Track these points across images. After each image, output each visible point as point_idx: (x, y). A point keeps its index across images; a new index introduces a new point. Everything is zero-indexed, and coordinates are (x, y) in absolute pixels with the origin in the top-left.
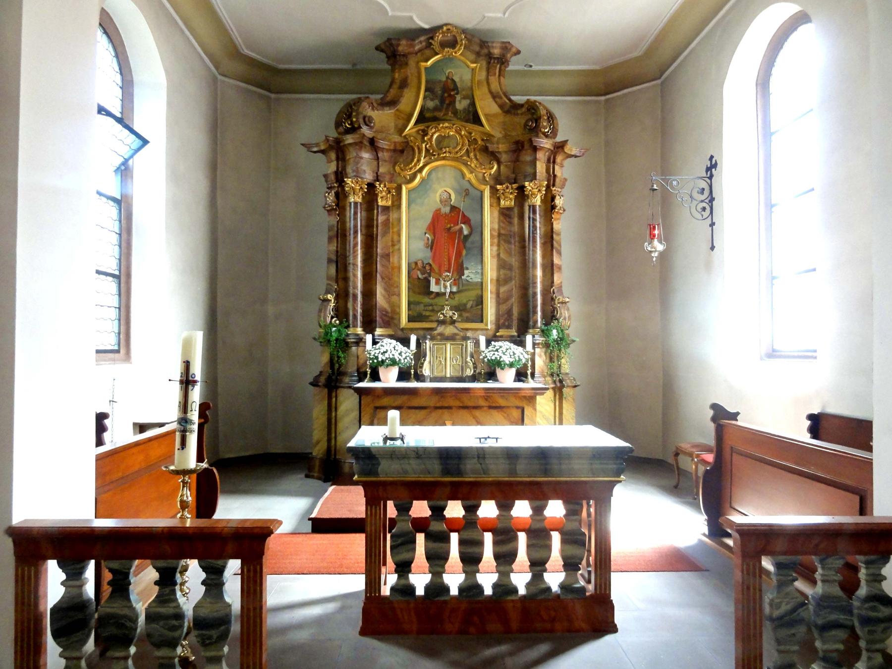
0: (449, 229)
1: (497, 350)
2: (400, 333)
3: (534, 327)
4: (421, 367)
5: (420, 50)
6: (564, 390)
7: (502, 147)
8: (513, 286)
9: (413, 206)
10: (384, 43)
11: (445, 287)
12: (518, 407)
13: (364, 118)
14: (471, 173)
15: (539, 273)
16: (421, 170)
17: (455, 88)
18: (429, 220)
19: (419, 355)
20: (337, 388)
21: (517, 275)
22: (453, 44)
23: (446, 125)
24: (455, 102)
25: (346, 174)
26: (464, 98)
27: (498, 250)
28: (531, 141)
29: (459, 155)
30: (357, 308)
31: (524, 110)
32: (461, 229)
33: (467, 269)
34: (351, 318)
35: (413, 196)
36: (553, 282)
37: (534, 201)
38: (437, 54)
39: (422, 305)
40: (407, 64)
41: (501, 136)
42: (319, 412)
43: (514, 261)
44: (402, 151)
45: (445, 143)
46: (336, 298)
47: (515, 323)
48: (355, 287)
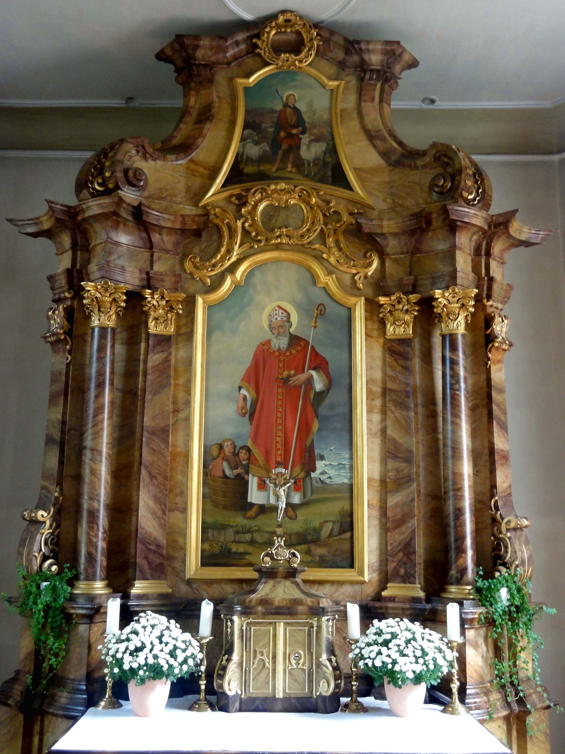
0: (286, 380)
2: (184, 589)
3: (459, 581)
4: (222, 677)
5: (236, 58)
6: (530, 720)
7: (389, 226)
8: (415, 493)
9: (217, 335)
10: (171, 45)
11: (278, 497)
14: (330, 273)
15: (466, 468)
16: (232, 269)
17: (300, 122)
19: (219, 648)
21: (422, 472)
22: (296, 47)
23: (282, 185)
24: (298, 147)
25: (88, 274)
26: (318, 139)
27: (383, 420)
28: (445, 211)
29: (305, 241)
30: (95, 538)
31: (427, 159)
32: (309, 382)
33: (322, 458)
34: (83, 559)
35: (218, 315)
36: (493, 486)
37: (453, 325)
38: (267, 64)
39: (230, 532)
40: (211, 81)
43: (416, 444)
44: (197, 234)
45: (280, 221)
46: (57, 518)
47: (419, 570)
48: (94, 497)
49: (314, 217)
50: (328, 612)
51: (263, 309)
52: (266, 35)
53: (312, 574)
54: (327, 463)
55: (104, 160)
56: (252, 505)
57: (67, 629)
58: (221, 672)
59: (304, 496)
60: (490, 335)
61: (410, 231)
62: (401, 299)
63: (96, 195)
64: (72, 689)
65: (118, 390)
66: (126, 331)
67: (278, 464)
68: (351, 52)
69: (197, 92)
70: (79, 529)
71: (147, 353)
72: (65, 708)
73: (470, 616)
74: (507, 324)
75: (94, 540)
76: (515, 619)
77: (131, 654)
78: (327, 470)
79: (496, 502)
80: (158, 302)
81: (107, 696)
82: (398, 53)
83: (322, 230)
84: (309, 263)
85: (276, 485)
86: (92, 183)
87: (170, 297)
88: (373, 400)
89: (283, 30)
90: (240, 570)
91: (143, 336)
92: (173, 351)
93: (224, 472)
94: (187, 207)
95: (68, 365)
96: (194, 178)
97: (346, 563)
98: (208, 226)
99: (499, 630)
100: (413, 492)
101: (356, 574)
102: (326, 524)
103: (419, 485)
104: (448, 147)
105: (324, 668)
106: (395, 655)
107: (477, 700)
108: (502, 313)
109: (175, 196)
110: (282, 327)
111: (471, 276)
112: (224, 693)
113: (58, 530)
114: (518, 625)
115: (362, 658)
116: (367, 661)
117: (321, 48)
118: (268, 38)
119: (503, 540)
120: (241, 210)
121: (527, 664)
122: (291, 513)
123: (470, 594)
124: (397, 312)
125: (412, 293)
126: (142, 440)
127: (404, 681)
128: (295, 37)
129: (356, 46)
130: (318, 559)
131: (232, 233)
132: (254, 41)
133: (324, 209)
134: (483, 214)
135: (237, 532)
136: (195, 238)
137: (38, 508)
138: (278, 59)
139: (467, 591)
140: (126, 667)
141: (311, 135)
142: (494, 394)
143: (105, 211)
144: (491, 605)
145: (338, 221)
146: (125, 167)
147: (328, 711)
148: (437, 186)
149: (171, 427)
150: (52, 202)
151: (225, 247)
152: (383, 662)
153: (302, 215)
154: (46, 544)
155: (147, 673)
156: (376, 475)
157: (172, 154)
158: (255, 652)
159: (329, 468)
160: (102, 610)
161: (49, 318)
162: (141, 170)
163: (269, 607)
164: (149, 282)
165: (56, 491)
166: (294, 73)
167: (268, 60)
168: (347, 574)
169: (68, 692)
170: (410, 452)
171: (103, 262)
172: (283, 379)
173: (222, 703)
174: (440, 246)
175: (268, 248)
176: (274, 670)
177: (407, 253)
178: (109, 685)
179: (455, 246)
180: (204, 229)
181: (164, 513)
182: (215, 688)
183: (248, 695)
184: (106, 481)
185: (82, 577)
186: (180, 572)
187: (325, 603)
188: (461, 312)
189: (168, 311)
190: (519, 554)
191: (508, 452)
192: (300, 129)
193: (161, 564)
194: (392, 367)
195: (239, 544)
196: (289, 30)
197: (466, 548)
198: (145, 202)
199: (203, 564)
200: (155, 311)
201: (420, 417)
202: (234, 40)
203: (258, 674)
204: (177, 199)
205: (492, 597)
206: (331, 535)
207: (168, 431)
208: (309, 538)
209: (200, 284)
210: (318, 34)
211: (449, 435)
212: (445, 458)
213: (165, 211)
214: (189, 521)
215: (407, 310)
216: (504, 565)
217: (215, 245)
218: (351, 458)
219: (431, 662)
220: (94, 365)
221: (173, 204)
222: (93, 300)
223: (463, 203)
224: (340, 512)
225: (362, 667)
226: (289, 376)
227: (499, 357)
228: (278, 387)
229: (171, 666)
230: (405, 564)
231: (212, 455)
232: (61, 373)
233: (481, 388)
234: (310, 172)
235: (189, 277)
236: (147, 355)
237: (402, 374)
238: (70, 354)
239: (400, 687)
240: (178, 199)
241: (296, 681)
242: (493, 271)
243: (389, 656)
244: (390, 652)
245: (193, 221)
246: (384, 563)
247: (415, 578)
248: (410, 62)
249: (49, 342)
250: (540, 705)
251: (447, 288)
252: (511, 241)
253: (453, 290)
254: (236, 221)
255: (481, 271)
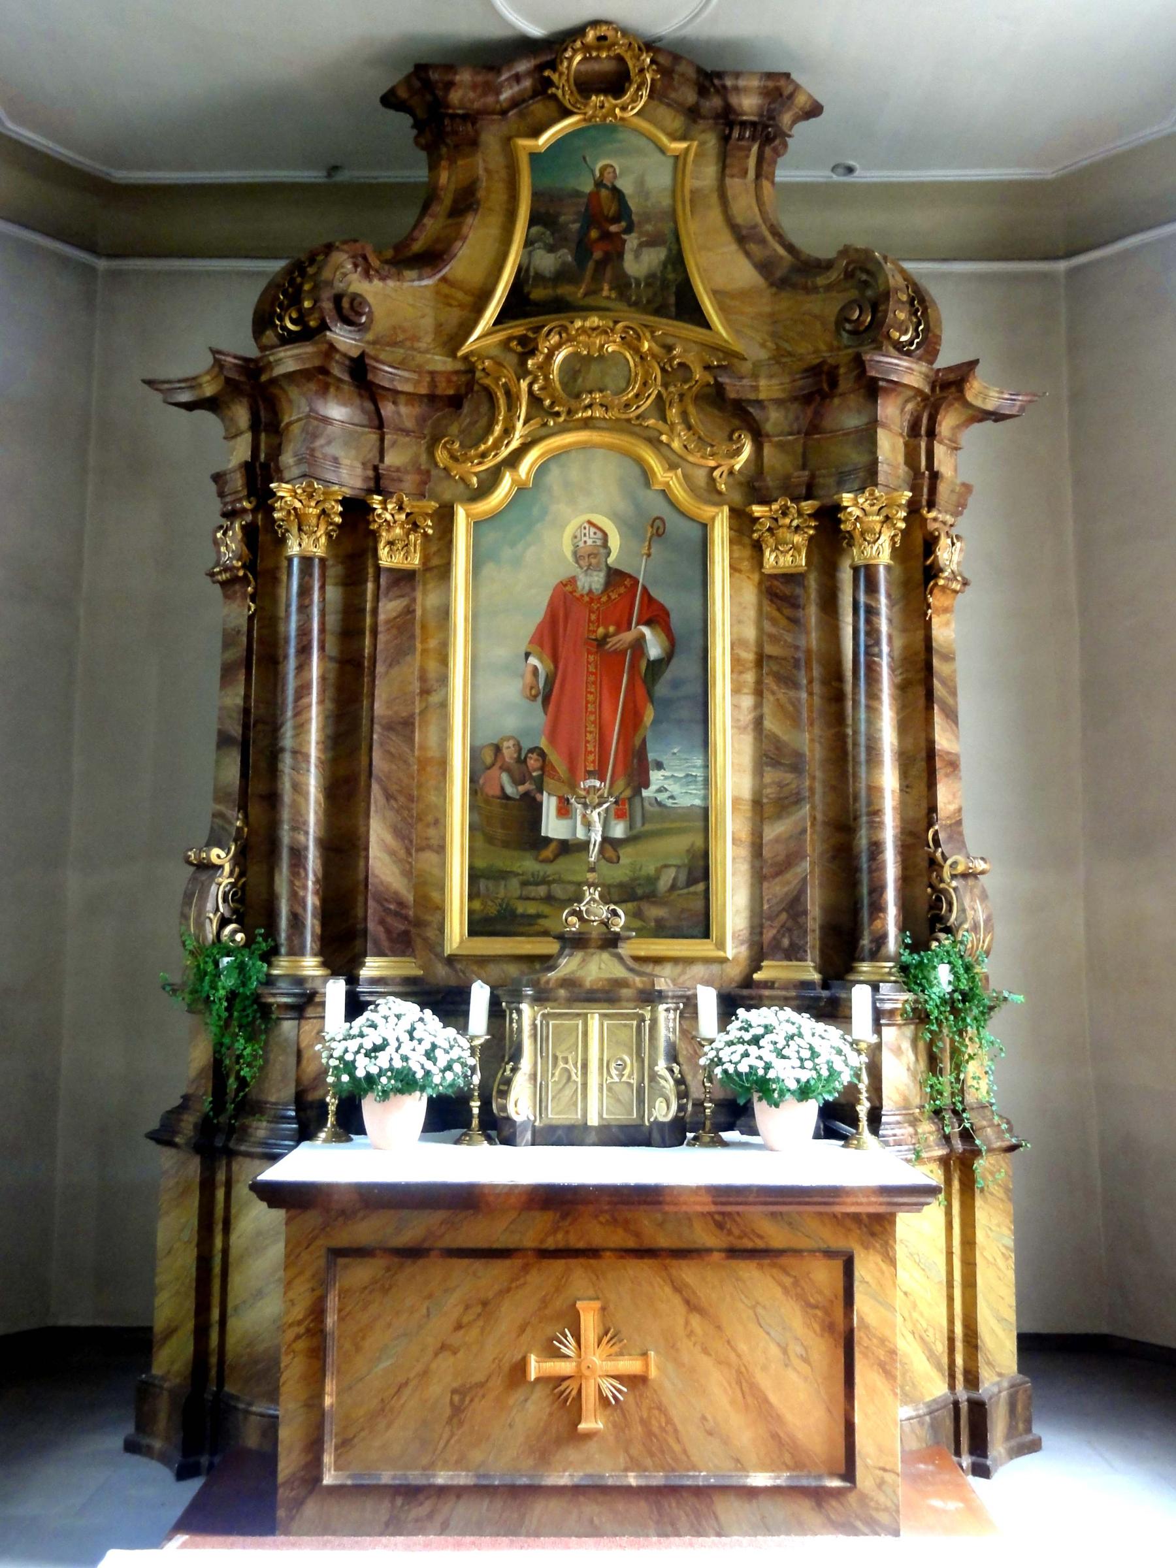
0: (602, 642)
1: (756, 1041)
2: (441, 972)
3: (876, 954)
4: (504, 1094)
5: (515, 103)
6: (981, 1165)
7: (768, 387)
8: (806, 821)
9: (488, 570)
10: (408, 80)
11: (588, 825)
12: (829, 1254)
13: (338, 299)
14: (672, 467)
15: (889, 779)
16: (513, 460)
17: (623, 211)
18: (538, 614)
19: (499, 1052)
20: (231, 1154)
22: (616, 83)
23: (594, 321)
24: (620, 255)
25: (279, 470)
26: (653, 242)
27: (758, 705)
28: (859, 363)
29: (633, 413)
30: (303, 891)
31: (834, 275)
32: (639, 645)
33: (659, 766)
34: (283, 923)
35: (491, 536)
36: (933, 809)
38: (566, 113)
39: (514, 883)
40: (474, 143)
41: (763, 355)
42: (174, 1230)
43: (809, 742)
44: (455, 402)
45: (593, 374)
46: (241, 860)
47: (813, 940)
48: (299, 826)
49: (647, 374)
50: (667, 997)
51: (563, 528)
52: (565, 64)
53: (644, 946)
54: (667, 774)
55: (299, 280)
56: (548, 841)
57: (263, 1027)
58: (503, 1088)
59: (631, 827)
60: (931, 566)
61: (804, 396)
62: (788, 508)
63: (289, 339)
64: (275, 1117)
65: (331, 658)
66: (342, 563)
67: (590, 774)
68: (708, 91)
69: (452, 161)
70: (277, 878)
71: (376, 598)
72: (265, 1144)
73: (888, 1006)
74: (961, 550)
75: (301, 893)
76: (960, 1010)
77: (366, 1055)
78: (668, 784)
79: (936, 833)
80: (393, 515)
81: (329, 1125)
82: (786, 92)
83: (659, 396)
84: (637, 449)
85: (585, 806)
86: (281, 319)
87: (413, 507)
88: (741, 673)
89: (594, 54)
90: (529, 942)
91: (371, 570)
92: (419, 595)
93: (503, 789)
94: (437, 357)
95: (251, 619)
96: (448, 309)
97: (700, 929)
98: (472, 389)
99: (935, 1028)
100: (804, 819)
101: (712, 947)
102: (665, 870)
103: (813, 808)
104: (867, 253)
105: (662, 1082)
106: (770, 1057)
107: (897, 1131)
108: (953, 532)
109: (418, 339)
110: (596, 555)
111: (902, 470)
112: (508, 1119)
113: (243, 880)
114: (964, 1020)
115: (720, 1062)
116: (725, 1066)
117: (659, 84)
118: (569, 68)
119: (944, 892)
120: (526, 364)
121: (980, 1079)
122: (610, 853)
123: (890, 974)
124: (781, 530)
125: (807, 498)
126: (372, 739)
127: (782, 1094)
128: (612, 65)
129: (716, 82)
130: (653, 924)
131: (512, 399)
132: (546, 73)
133: (662, 359)
134: (923, 367)
135: (524, 884)
136: (451, 409)
137: (210, 844)
138: (585, 105)
139: (887, 970)
140: (360, 1073)
141: (641, 234)
142: (936, 662)
143: (307, 366)
144: (923, 991)
145: (685, 381)
146: (334, 291)
147: (668, 1142)
148: (849, 321)
149: (417, 719)
150: (219, 352)
151: (500, 424)
152: (751, 1067)
153: (626, 369)
154: (225, 900)
155: (393, 1082)
156: (746, 793)
157: (412, 268)
158: (555, 1058)
159: (670, 781)
160: (317, 999)
161: (216, 543)
162: (360, 296)
163: (576, 990)
164: (378, 483)
165: (238, 819)
166: (612, 129)
167: (569, 107)
168: (699, 948)
169: (268, 1122)
170: (799, 755)
171: (303, 450)
172: (596, 640)
173: (506, 1132)
174: (852, 420)
175: (571, 425)
176: (585, 1085)
177: (799, 433)
178: (332, 1108)
179: (876, 421)
180: (467, 394)
181: (409, 853)
182: (495, 1111)
183: (545, 1121)
184: (317, 802)
185: (283, 950)
186: (435, 946)
187: (662, 984)
188: (884, 529)
189: (410, 530)
190: (970, 914)
191: (957, 755)
192: (623, 224)
193: (406, 933)
194: (773, 621)
195: (528, 902)
196: (604, 55)
197: (886, 903)
198: (370, 350)
199: (472, 933)
200: (388, 531)
201: (817, 700)
202: (513, 72)
203: (561, 1090)
204: (420, 345)
205: (924, 978)
206: (673, 887)
207: (413, 724)
208: (640, 892)
209: (461, 486)
210: (653, 62)
211: (863, 727)
212: (856, 763)
213: (401, 365)
214: (448, 865)
215: (797, 527)
216: (948, 930)
217: (483, 422)
218: (706, 766)
219: (825, 1067)
220: (294, 618)
221: (415, 353)
222: (289, 512)
223: (891, 349)
224: (688, 851)
225: (719, 1076)
226: (606, 636)
227: (946, 603)
228: (589, 653)
229: (428, 1073)
230: (790, 930)
231: (483, 762)
232: (239, 632)
233: (916, 654)
234: (639, 297)
235: (442, 474)
236: (378, 601)
237: (788, 631)
238: (253, 601)
239: (777, 1106)
240: (422, 345)
241: (619, 1100)
242: (940, 462)
243: (760, 1058)
244: (761, 1052)
245: (449, 381)
246: (758, 930)
247: (806, 951)
248: (807, 108)
249: (219, 582)
250: (998, 1144)
251: (862, 490)
252: (970, 412)
253: (872, 494)
254: (519, 380)
255: (920, 462)
